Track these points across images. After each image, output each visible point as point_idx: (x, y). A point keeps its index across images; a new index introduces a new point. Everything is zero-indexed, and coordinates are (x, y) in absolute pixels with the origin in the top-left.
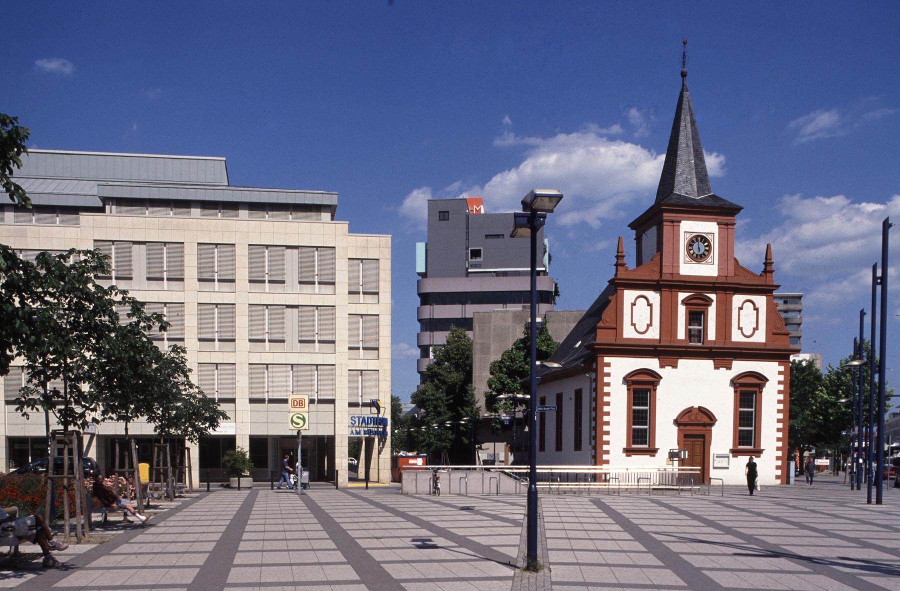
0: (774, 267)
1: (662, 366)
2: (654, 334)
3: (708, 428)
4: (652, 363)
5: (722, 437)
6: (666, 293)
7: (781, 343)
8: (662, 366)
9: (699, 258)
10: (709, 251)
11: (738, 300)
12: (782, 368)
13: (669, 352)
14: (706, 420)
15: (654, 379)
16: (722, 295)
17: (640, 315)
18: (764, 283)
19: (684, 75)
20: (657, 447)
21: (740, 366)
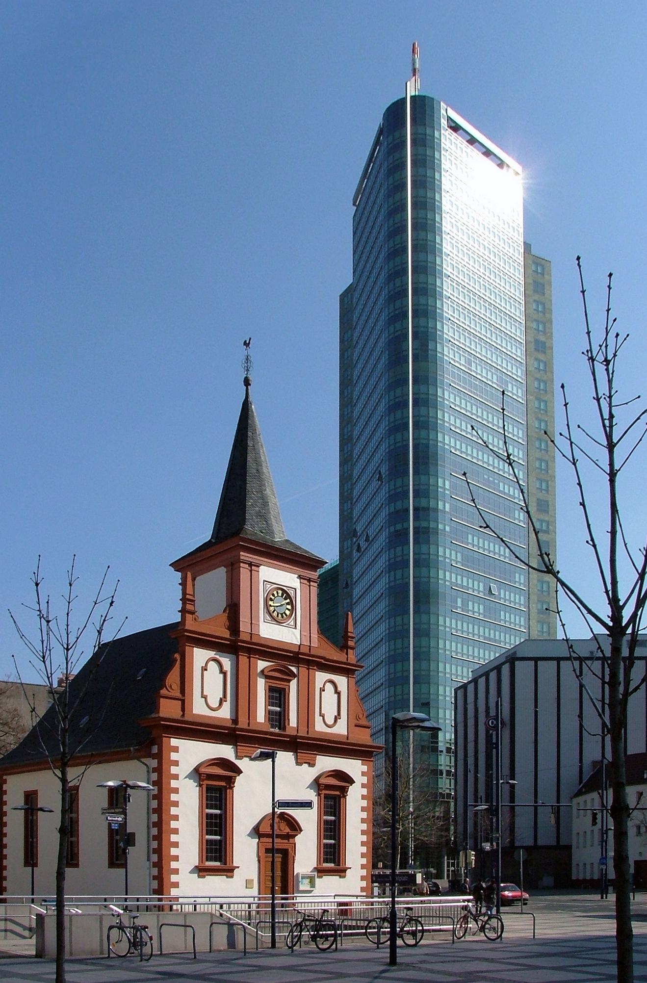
1: (238, 757)
2: (225, 713)
4: (226, 751)
5: (306, 852)
6: (243, 659)
8: (238, 757)
9: (278, 619)
17: (207, 683)
18: (345, 660)
19: (247, 382)
21: (326, 763)
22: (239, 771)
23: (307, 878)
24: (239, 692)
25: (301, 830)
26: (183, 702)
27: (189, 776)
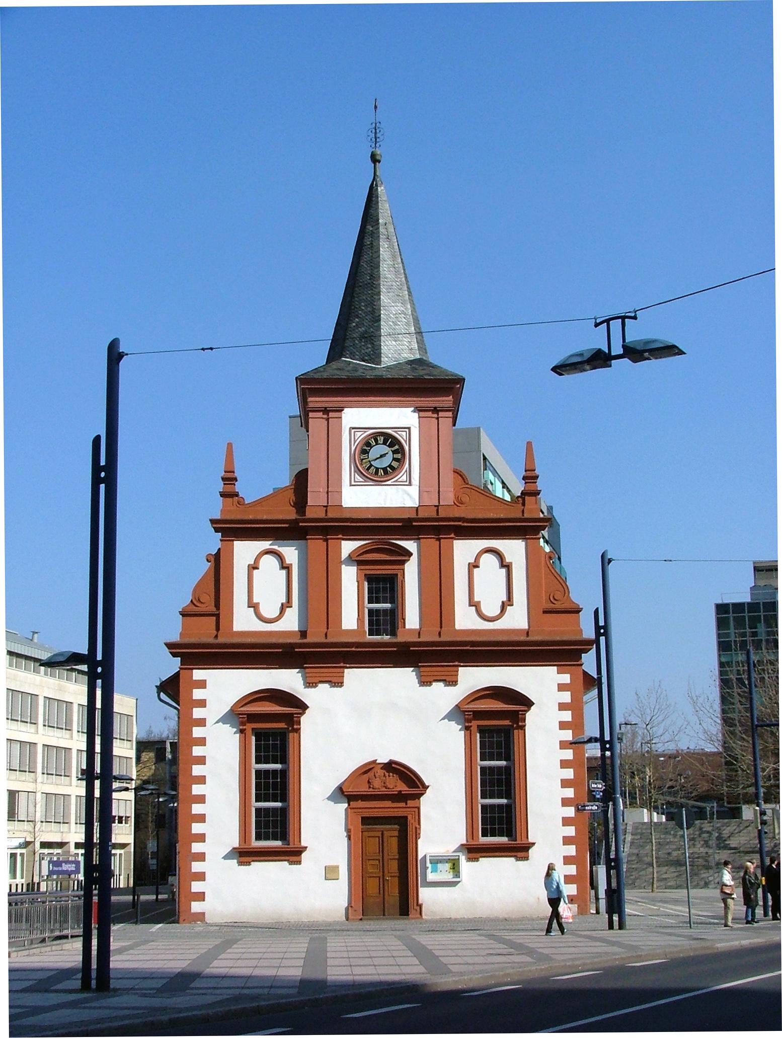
0: (540, 484)
1: (310, 684)
4: (288, 679)
5: (443, 820)
6: (316, 544)
10: (400, 461)
11: (464, 550)
12: (566, 678)
13: (322, 655)
14: (402, 787)
16: (430, 543)
18: (519, 515)
19: (375, 159)
20: (303, 844)
21: (475, 678)
22: (303, 707)
23: (447, 861)
24: (319, 594)
25: (426, 787)
26: (218, 616)
27: (224, 720)
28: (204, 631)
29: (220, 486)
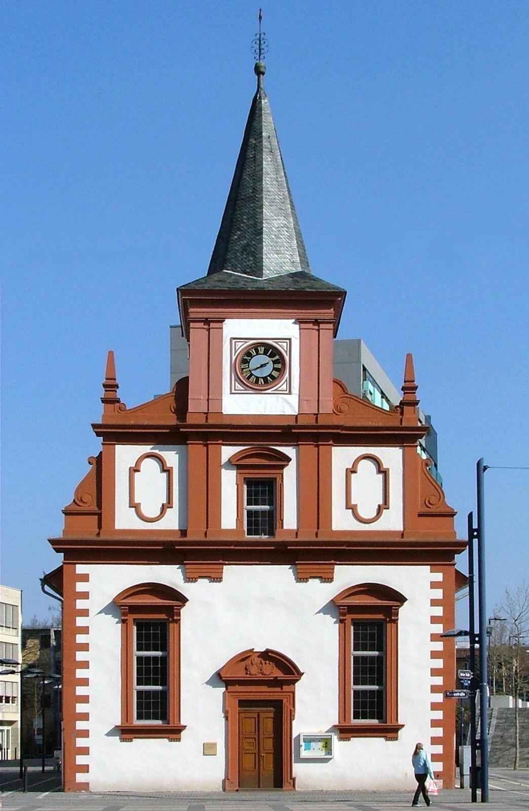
0: (419, 395)
1: (189, 579)
2: (171, 522)
3: (285, 688)
4: (169, 575)
5: (316, 704)
6: (197, 449)
7: (431, 531)
9: (259, 384)
10: (281, 371)
11: (342, 456)
12: (439, 577)
13: (202, 553)
15: (173, 600)
16: (309, 449)
18: (397, 424)
19: (258, 71)
20: (183, 723)
21: (349, 575)
22: (183, 600)
23: (320, 740)
24: (199, 495)
26: (100, 515)
27: (106, 610)
28: (86, 529)
29: (102, 393)
